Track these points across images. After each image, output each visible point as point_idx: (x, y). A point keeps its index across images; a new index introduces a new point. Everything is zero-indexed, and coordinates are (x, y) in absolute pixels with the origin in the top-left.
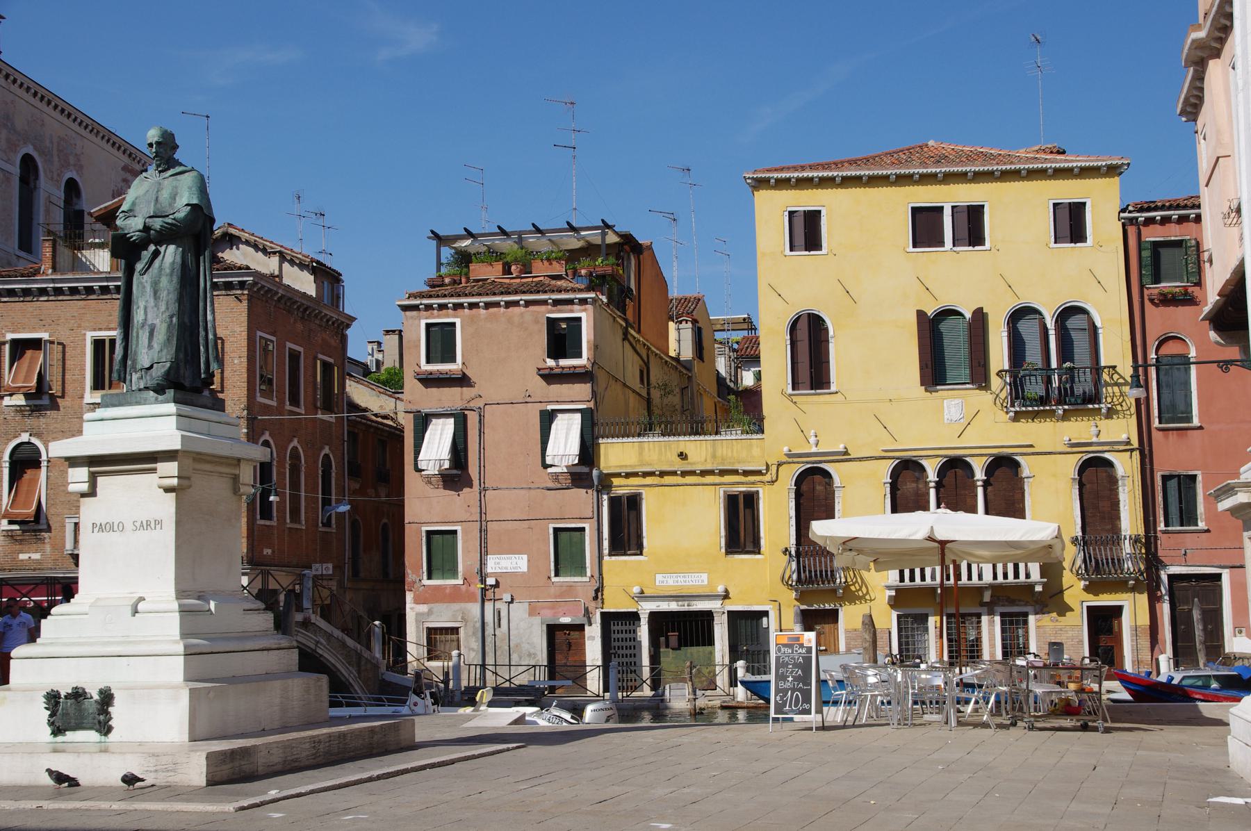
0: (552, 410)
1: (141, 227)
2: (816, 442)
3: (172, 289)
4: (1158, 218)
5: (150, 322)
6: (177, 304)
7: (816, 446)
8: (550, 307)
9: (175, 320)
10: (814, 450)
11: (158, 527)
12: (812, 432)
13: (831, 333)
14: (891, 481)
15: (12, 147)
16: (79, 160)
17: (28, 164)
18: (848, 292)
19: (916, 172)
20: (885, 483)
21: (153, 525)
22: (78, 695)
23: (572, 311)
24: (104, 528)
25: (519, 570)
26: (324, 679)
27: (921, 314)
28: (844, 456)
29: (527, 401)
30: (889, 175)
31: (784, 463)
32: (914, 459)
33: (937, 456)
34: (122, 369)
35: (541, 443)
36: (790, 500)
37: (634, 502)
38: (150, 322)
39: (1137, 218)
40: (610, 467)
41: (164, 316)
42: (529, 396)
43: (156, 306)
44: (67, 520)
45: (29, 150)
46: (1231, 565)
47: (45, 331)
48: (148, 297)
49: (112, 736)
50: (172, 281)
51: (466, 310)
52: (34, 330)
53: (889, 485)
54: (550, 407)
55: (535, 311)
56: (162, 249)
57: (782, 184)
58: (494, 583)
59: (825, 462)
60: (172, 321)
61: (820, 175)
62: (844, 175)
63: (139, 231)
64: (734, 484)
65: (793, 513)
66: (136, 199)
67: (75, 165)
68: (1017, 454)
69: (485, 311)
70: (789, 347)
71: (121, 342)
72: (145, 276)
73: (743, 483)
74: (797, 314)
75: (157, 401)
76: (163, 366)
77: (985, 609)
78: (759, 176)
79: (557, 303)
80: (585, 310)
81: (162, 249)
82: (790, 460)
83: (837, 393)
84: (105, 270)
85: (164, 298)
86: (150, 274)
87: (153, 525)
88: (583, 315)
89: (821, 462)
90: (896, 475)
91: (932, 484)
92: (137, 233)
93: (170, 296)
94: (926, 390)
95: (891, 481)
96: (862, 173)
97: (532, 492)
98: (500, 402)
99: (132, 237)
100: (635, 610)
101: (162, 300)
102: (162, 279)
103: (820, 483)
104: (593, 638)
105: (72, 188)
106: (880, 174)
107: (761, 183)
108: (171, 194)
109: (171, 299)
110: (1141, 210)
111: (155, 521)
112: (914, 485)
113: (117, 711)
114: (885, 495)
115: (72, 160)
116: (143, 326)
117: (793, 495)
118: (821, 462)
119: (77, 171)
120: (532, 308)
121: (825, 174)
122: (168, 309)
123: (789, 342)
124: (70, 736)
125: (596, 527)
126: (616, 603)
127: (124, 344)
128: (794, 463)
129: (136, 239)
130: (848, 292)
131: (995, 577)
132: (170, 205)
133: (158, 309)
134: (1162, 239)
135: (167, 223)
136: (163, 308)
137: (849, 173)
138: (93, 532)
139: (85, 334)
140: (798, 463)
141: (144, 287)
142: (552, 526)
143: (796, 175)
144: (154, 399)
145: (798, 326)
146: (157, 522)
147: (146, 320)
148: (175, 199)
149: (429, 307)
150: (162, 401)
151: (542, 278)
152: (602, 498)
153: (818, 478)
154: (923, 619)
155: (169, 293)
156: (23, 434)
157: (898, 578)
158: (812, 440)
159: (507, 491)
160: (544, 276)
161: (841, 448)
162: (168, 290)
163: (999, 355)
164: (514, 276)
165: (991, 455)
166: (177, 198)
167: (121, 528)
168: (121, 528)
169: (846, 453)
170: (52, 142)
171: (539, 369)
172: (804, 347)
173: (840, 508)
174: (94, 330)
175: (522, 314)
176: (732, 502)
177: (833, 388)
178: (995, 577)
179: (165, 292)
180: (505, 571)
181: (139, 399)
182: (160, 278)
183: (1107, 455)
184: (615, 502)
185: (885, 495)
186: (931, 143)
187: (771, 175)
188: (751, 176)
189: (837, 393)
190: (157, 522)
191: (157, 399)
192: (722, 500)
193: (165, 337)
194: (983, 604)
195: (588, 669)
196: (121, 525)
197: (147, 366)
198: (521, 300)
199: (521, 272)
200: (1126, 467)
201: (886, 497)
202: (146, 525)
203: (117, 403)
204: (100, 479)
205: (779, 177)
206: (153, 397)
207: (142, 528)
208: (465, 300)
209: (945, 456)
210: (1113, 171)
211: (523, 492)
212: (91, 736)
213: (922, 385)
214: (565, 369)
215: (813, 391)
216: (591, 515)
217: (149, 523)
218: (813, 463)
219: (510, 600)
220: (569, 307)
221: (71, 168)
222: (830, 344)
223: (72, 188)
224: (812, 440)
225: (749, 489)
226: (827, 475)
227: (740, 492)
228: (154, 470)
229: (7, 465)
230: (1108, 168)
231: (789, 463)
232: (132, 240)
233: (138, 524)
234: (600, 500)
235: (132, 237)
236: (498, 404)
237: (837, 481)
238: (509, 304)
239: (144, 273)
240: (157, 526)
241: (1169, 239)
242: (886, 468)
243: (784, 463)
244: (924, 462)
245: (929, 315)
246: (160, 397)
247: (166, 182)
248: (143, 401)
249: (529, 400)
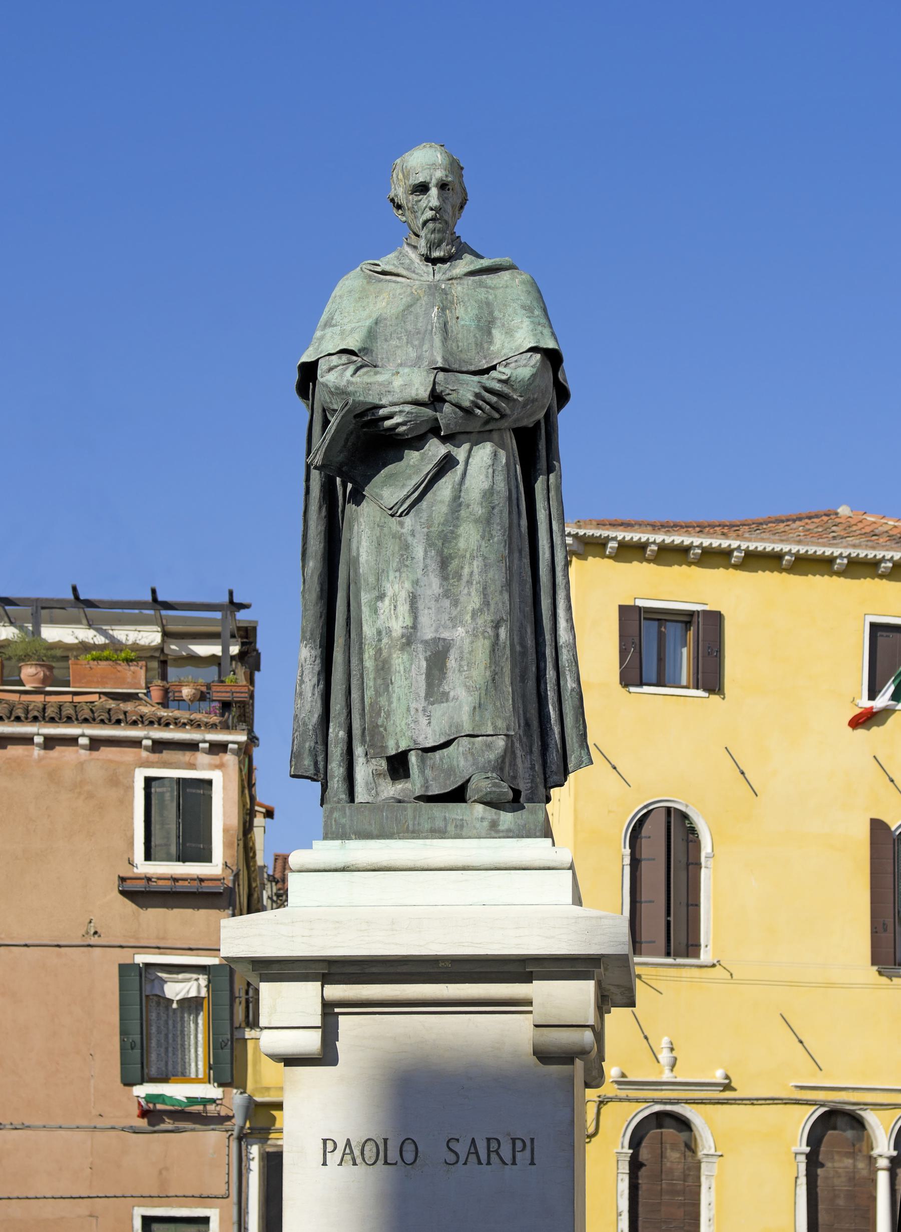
0: (148, 965)
2: (670, 1061)
3: (492, 557)
5: (427, 632)
6: (506, 596)
7: (672, 1070)
8: (144, 754)
9: (503, 632)
10: (667, 1076)
11: (523, 1157)
12: (665, 1042)
13: (706, 847)
14: (808, 1149)
18: (743, 773)
19: (888, 557)
20: (796, 1154)
23: (192, 766)
24: (357, 1153)
29: (92, 943)
30: (836, 558)
31: (611, 1100)
33: (807, 1103)
34: (320, 747)
35: (121, 1034)
36: (620, 1176)
38: (427, 632)
40: (268, 1089)
41: (480, 621)
42: (96, 933)
43: (447, 594)
48: (420, 572)
50: (492, 537)
53: (803, 1158)
54: (141, 959)
55: (111, 761)
56: (460, 454)
59: (688, 1102)
60: (497, 636)
61: (706, 542)
62: (752, 548)
63: (416, 403)
66: (376, 323)
69: (42, 752)
70: (627, 870)
71: (315, 680)
72: (408, 520)
74: (645, 807)
75: (494, 831)
76: (489, 746)
78: (590, 532)
79: (159, 746)
80: (220, 766)
81: (460, 454)
82: (622, 1094)
83: (714, 966)
85: (476, 577)
86: (425, 515)
88: (216, 776)
89: (677, 1102)
90: (815, 1138)
91: (883, 1163)
92: (408, 408)
93: (490, 575)
94: (880, 973)
95: (808, 1149)
97: (99, 1136)
98: (29, 942)
99: (390, 417)
101: (469, 582)
102: (461, 530)
103: (674, 1147)
106: (819, 553)
108: (479, 319)
109: (493, 580)
111: (514, 1140)
112: (848, 1162)
114: (797, 1178)
116: (409, 643)
117: (625, 1168)
118: (677, 1102)
120: (107, 753)
121: (715, 543)
122: (486, 603)
123: (627, 860)
125: (235, 1217)
127: (321, 686)
128: (629, 1100)
129: (403, 424)
130: (743, 773)
132: (479, 346)
133: (456, 603)
135: (487, 390)
136: (474, 601)
137: (760, 546)
138: (324, 1164)
140: (637, 1100)
141: (406, 547)
143: (659, 538)
144: (486, 824)
145: (646, 830)
146: (519, 1144)
147: (414, 627)
148: (489, 333)
150: (509, 830)
151: (95, 698)
152: (248, 1153)
153: (669, 1132)
155: (486, 566)
158: (665, 1056)
159: (43, 1133)
160: (100, 693)
161: (718, 1076)
162: (485, 558)
164: (27, 688)
166: (494, 331)
168: (409, 1156)
169: (728, 1087)
171: (122, 879)
172: (654, 873)
173: (713, 1199)
175: (81, 765)
177: (706, 956)
179: (477, 564)
181: (439, 824)
182: (456, 526)
185: (797, 1178)
186: (844, 510)
187: (612, 534)
189: (714, 966)
190: (519, 1144)
191: (494, 825)
193: (488, 673)
196: (409, 1147)
197: (430, 744)
198: (83, 735)
199: (46, 681)
201: (799, 1182)
203: (374, 829)
204: (346, 1024)
205: (627, 538)
206: (482, 819)
207: (473, 1158)
211: (79, 1135)
213: (873, 963)
214: (181, 883)
215: (670, 960)
216: (222, 1191)
217: (494, 1145)
218: (665, 1103)
220: (187, 756)
222: (703, 871)
224: (665, 1056)
226: (684, 1124)
228: (523, 1004)
230: (894, 565)
231: (621, 1100)
232: (388, 423)
233: (462, 1148)
234: (244, 1158)
235: (390, 417)
236: (26, 945)
237: (707, 1143)
238: (50, 742)
239: (408, 512)
240: (518, 1155)
242: (805, 1117)
243: (611, 1100)
244: (871, 1118)
245: (893, 829)
246: (507, 818)
247: (458, 289)
248: (451, 828)
249: (94, 940)
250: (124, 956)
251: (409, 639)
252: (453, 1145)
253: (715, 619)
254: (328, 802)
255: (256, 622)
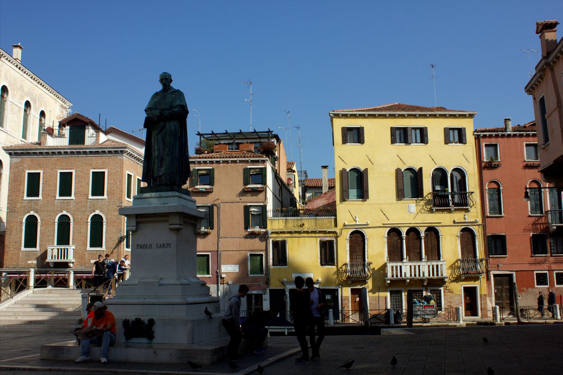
1: (158, 114)
4: (488, 135)
11: (168, 247)
15: (22, 97)
16: (46, 103)
17: (28, 104)
21: (166, 246)
22: (138, 321)
25: (235, 271)
26: (89, 319)
27: (398, 171)
28: (366, 226)
32: (397, 227)
33: (407, 227)
37: (284, 243)
39: (480, 135)
44: (48, 248)
45: (28, 99)
46: (516, 270)
47: (41, 170)
49: (154, 341)
51: (238, 164)
52: (36, 169)
54: (248, 204)
57: (345, 116)
58: (222, 276)
64: (323, 237)
65: (366, 247)
67: (44, 105)
68: (437, 226)
73: (328, 237)
75: (167, 191)
77: (424, 289)
79: (253, 162)
84: (66, 145)
87: (166, 246)
89: (359, 228)
96: (376, 113)
100: (284, 288)
104: (266, 300)
105: (43, 114)
107: (337, 116)
110: (482, 131)
113: (157, 330)
115: (43, 103)
118: (359, 228)
119: (45, 108)
121: (392, 113)
124: (134, 340)
126: (275, 285)
128: (350, 228)
131: (429, 275)
134: (489, 143)
139: (57, 171)
142: (263, 253)
143: (350, 113)
149: (528, 136)
154: (400, 292)
156: (31, 212)
157: (410, 275)
163: (427, 187)
165: (427, 226)
167: (150, 247)
168: (150, 247)
170: (36, 96)
174: (108, 173)
176: (323, 245)
178: (429, 275)
180: (229, 272)
183: (470, 227)
184: (275, 244)
188: (332, 113)
192: (319, 243)
194: (423, 286)
195: (241, 312)
196: (150, 246)
198: (196, 161)
200: (478, 231)
202: (162, 246)
208: (531, 133)
209: (409, 227)
210: (471, 116)
211: (237, 239)
212: (144, 340)
219: (229, 284)
221: (43, 106)
223: (43, 114)
225: (330, 239)
227: (327, 240)
228: (166, 221)
229: (24, 224)
233: (159, 245)
241: (491, 143)
249: (240, 201)
250: (245, 204)
251: (158, 156)
252: (158, 245)
253: (362, 129)
254: (288, 173)
255: (465, 143)
